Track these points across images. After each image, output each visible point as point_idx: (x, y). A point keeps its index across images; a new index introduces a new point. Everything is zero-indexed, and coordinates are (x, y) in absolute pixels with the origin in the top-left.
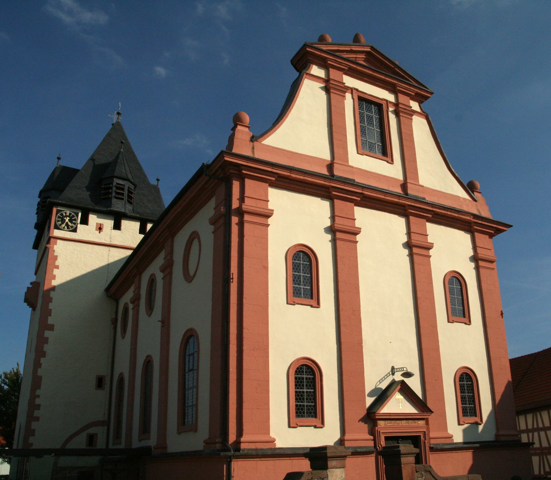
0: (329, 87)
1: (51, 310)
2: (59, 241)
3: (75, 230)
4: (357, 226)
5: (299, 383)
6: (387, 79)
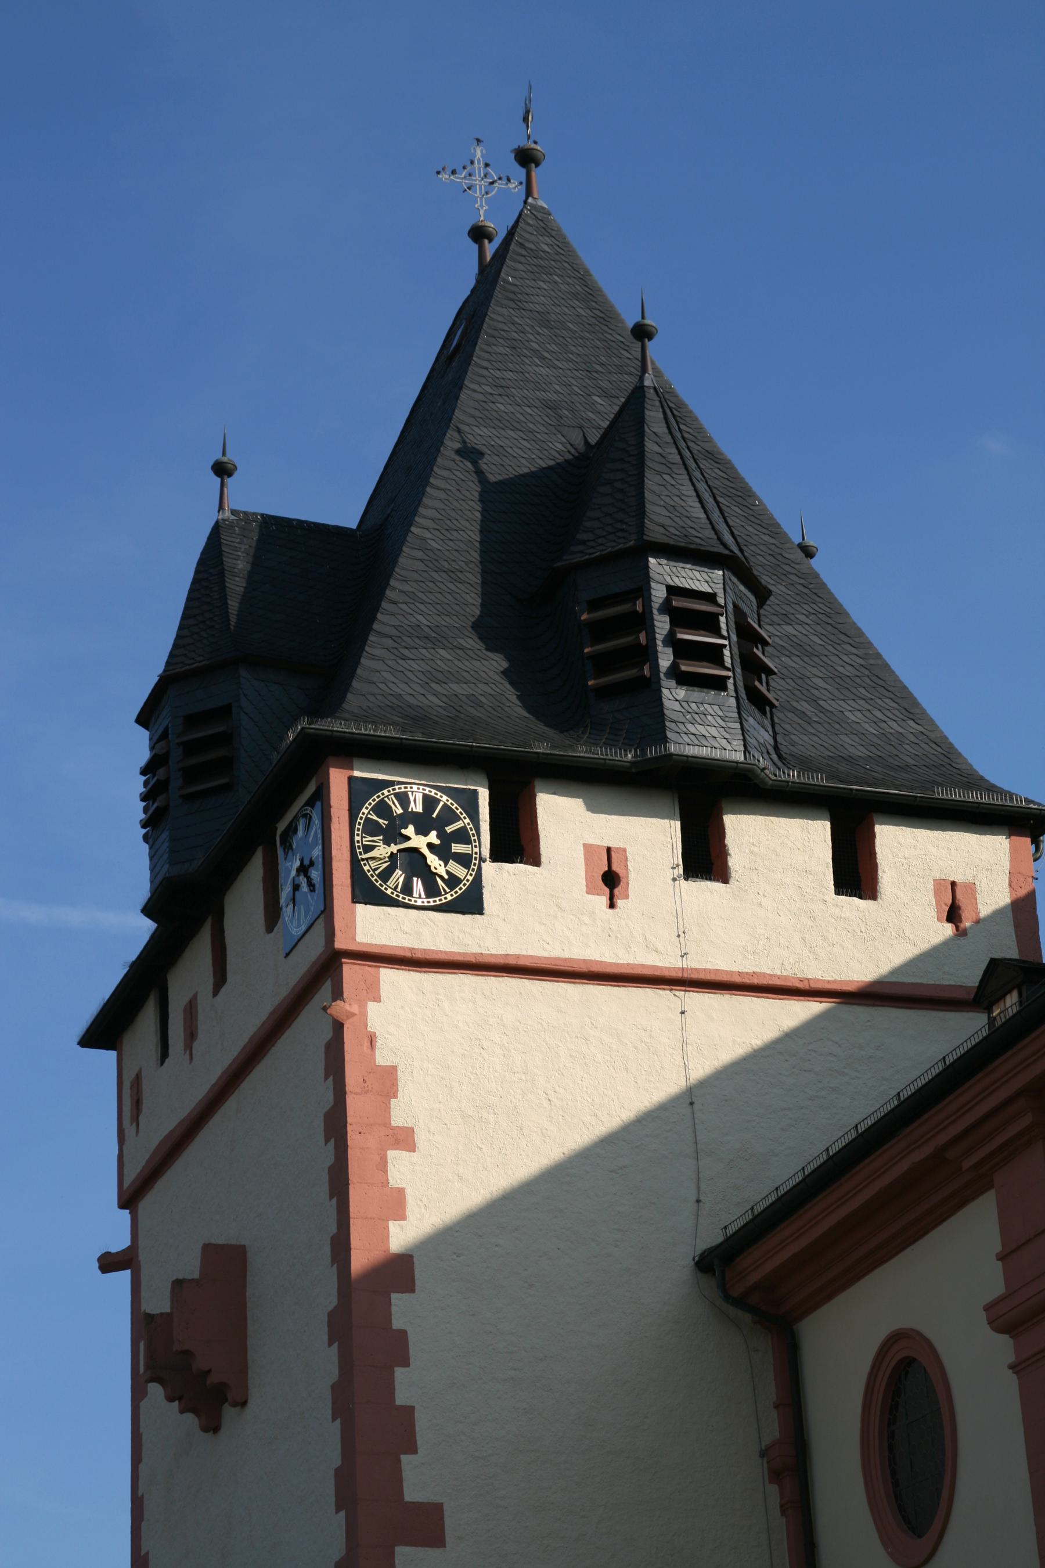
1: (409, 1411)
2: (388, 976)
3: (471, 902)
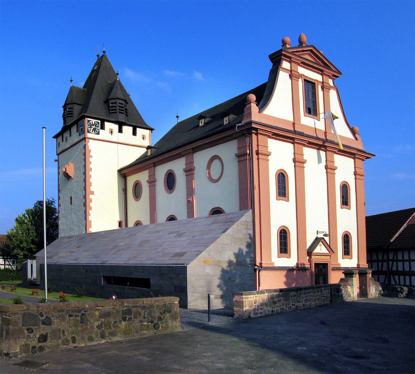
0: (293, 75)
2: (90, 140)
3: (98, 134)
4: (304, 159)
5: (281, 236)
6: (319, 67)
